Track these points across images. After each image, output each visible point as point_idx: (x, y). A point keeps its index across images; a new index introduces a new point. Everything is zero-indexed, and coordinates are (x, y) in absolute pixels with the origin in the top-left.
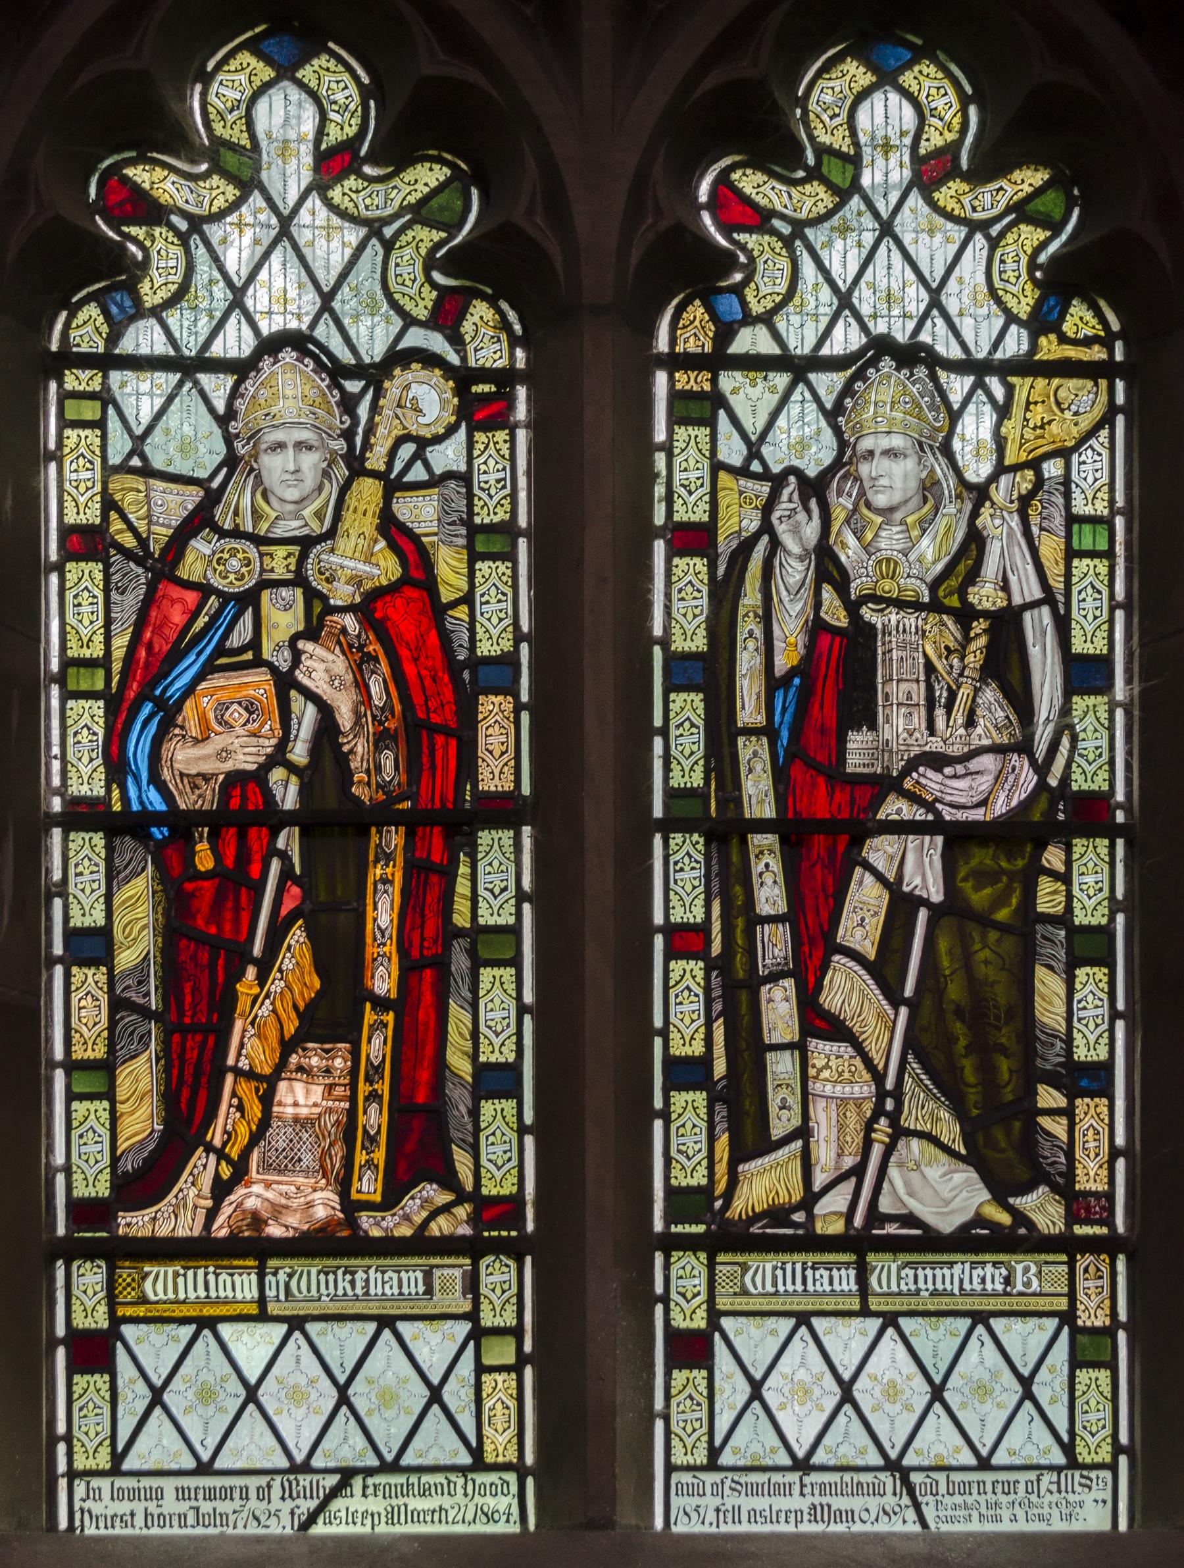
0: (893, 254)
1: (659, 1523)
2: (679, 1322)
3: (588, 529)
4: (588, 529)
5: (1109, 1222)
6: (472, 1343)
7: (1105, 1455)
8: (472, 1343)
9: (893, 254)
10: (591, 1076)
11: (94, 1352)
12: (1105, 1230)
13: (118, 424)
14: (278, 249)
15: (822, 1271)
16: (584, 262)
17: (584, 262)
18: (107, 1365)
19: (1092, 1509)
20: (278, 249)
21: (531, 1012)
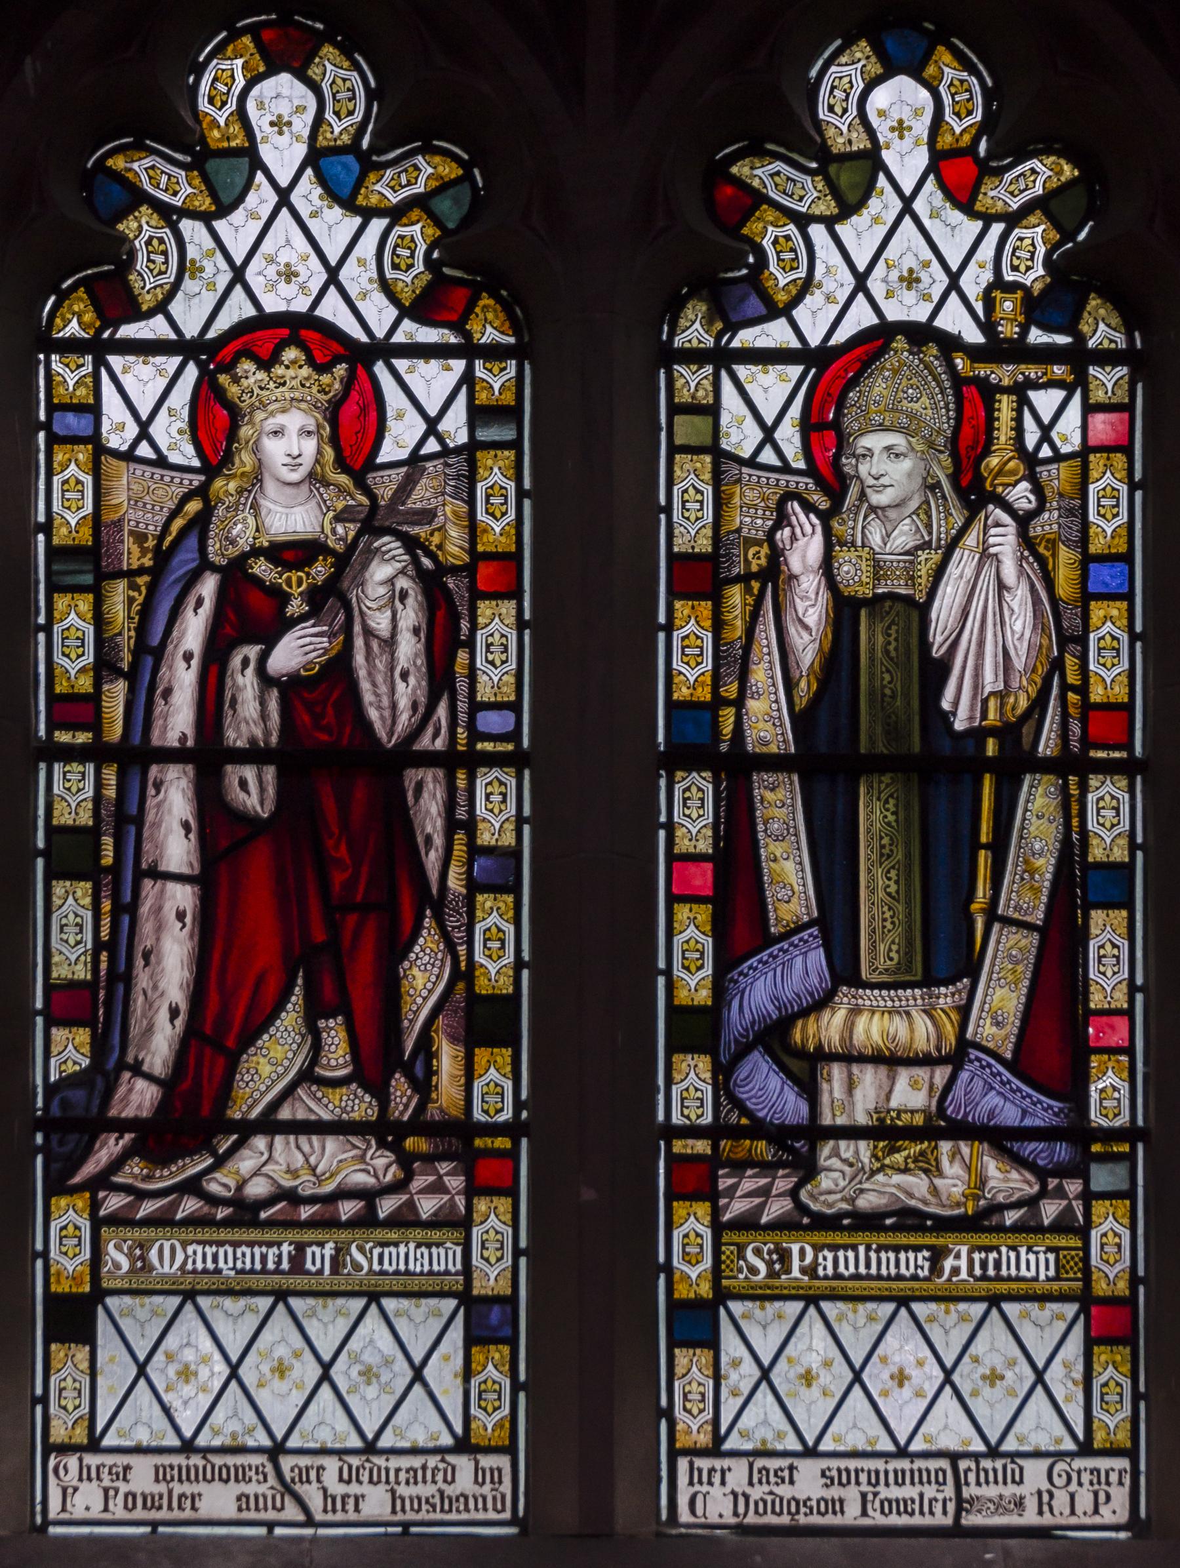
0: (901, 224)
1: (661, 1117)
2: (682, 997)
3: (594, 561)
4: (594, 561)
5: (1129, 746)
6: (464, 389)
7: (1120, 1000)
8: (464, 389)
9: (901, 224)
10: (588, 1010)
11: (75, 1319)
12: (1124, 755)
13: (117, 399)
14: (285, 215)
15: (826, 1252)
16: (594, 221)
17: (594, 221)
18: (88, 1337)
19: (1100, 1503)
20: (285, 215)
21: (528, 497)
